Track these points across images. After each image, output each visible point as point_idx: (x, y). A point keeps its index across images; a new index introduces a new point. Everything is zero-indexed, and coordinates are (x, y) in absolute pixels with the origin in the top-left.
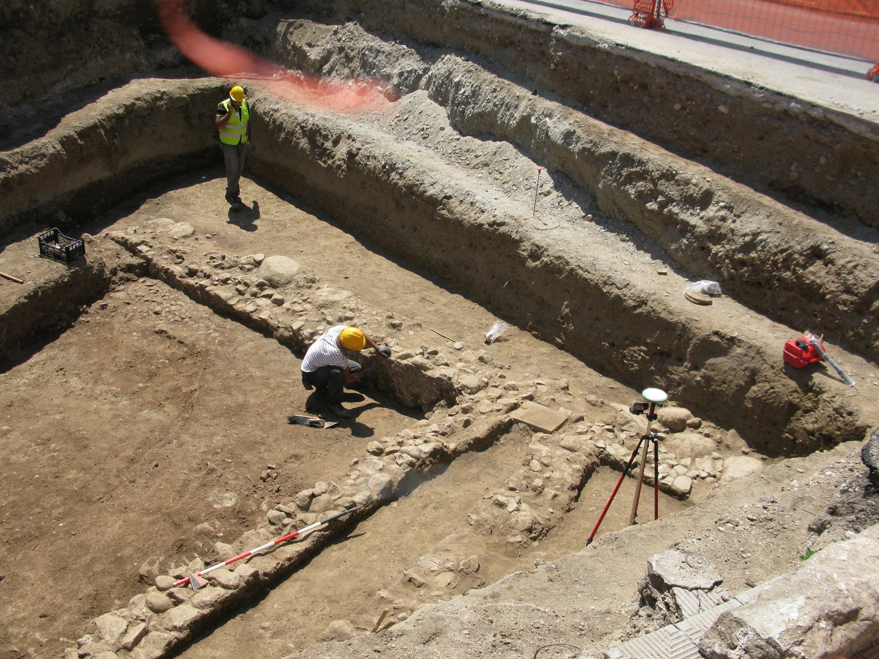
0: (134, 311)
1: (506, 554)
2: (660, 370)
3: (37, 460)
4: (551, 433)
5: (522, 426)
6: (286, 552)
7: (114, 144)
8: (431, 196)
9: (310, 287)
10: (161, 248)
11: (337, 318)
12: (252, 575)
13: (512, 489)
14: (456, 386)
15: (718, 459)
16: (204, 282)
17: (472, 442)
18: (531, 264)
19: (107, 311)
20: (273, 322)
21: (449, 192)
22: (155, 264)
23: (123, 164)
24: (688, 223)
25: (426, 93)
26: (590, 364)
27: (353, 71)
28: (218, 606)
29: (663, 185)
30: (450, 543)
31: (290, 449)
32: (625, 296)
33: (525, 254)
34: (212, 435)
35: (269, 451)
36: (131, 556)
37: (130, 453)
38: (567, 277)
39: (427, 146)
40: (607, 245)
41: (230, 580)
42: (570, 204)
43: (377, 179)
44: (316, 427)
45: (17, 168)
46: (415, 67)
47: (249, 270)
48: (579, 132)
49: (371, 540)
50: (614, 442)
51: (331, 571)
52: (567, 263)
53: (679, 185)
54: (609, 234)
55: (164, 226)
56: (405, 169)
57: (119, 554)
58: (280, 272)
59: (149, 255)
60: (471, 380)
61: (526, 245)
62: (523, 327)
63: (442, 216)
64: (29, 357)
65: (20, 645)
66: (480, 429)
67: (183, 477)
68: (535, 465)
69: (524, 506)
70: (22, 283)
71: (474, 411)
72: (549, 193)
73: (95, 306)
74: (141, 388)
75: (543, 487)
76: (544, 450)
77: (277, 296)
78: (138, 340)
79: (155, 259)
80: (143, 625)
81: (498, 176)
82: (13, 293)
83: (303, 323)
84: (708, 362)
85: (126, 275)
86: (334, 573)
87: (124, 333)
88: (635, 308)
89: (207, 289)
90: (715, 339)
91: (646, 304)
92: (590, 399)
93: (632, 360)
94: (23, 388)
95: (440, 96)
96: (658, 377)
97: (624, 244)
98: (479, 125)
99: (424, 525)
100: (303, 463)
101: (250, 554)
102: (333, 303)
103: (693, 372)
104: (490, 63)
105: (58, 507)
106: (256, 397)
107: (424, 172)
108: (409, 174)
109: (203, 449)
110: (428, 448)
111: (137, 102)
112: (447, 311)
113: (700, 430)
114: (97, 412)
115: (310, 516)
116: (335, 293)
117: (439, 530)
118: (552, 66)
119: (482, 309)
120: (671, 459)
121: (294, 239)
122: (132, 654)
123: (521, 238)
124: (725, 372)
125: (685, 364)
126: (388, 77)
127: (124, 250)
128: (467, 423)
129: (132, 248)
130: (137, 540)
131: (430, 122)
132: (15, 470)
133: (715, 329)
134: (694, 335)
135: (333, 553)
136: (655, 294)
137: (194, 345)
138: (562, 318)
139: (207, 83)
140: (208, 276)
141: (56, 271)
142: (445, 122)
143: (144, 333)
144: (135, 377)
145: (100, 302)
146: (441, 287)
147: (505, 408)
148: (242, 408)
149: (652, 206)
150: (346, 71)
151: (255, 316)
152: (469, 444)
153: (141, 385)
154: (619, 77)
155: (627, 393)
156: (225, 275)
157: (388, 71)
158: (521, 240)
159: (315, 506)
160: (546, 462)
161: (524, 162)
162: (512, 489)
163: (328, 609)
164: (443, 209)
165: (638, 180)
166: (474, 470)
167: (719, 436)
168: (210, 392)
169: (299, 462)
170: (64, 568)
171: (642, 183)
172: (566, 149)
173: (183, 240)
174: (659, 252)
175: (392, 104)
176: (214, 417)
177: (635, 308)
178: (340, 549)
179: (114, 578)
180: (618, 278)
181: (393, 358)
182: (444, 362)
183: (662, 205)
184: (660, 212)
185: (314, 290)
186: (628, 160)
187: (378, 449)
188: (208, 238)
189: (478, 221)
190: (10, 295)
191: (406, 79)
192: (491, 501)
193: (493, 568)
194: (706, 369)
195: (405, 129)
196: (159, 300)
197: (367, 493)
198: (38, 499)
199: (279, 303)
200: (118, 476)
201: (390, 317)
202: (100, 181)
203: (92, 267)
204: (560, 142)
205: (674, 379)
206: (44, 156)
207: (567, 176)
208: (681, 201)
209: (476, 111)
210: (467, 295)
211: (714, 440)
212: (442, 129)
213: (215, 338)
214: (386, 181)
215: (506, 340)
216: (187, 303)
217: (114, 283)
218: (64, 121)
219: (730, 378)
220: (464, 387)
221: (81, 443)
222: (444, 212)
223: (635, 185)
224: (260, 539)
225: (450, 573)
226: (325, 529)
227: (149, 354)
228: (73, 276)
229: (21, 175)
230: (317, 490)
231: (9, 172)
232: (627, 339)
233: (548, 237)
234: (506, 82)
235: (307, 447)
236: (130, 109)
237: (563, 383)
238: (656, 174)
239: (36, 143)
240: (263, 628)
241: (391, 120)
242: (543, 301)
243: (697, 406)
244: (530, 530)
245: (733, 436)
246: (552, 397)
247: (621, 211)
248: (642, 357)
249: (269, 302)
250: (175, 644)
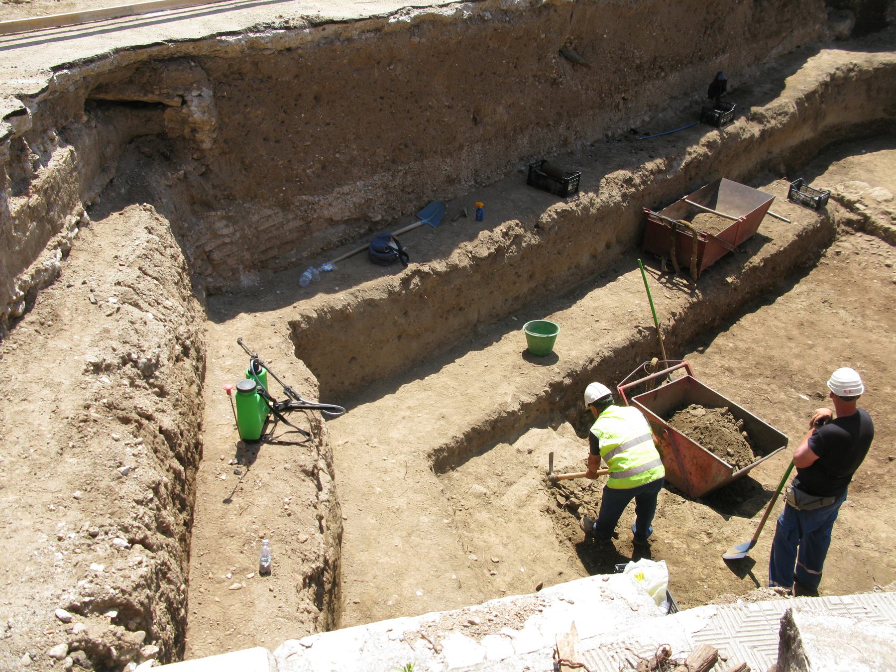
19: (840, 257)
22: (874, 222)
59: (868, 212)
79: (874, 218)
139: (888, 58)
206: (786, 113)
228: (822, 222)
229: (772, 128)
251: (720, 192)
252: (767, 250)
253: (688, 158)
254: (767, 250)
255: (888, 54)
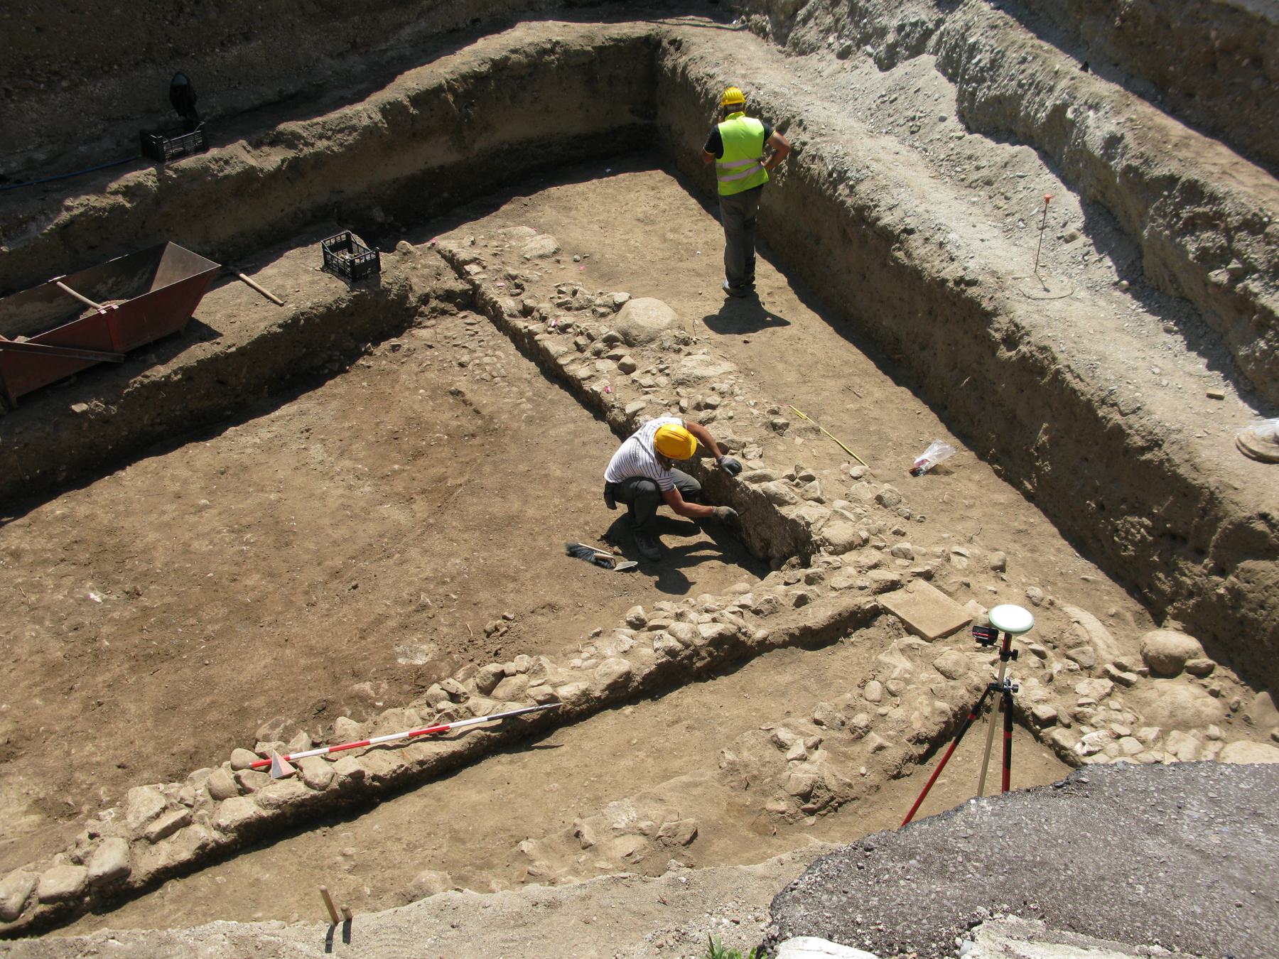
0: (433, 358)
1: (754, 827)
2: (1166, 564)
3: (220, 552)
4: (930, 640)
5: (891, 619)
6: (421, 751)
7: (468, 115)
8: (885, 227)
9: (679, 351)
10: (498, 271)
11: (694, 403)
12: (351, 775)
13: (818, 723)
14: (815, 538)
15: (1216, 739)
16: (534, 326)
17: (797, 633)
18: (1004, 353)
19: (397, 354)
20: (608, 398)
21: (911, 222)
22: (483, 294)
23: (481, 144)
24: (1271, 312)
25: (934, 58)
26: (1066, 534)
27: (838, 21)
28: (288, 810)
29: (1243, 241)
30: (672, 790)
31: (546, 594)
32: (1130, 428)
33: (998, 336)
34: (450, 555)
35: (518, 592)
36: (259, 709)
37: (338, 562)
38: (1050, 382)
39: (912, 146)
40: (1139, 336)
41: (317, 775)
42: (1100, 260)
43: (821, 193)
44: (603, 566)
45: (312, 145)
46: (924, 17)
47: (603, 315)
48: (1129, 139)
49: (564, 759)
50: (1033, 675)
51: (480, 792)
52: (1054, 359)
53: (1269, 244)
54: (1148, 318)
55: (521, 238)
56: (859, 181)
57: (246, 704)
58: (642, 323)
59: (477, 280)
60: (839, 532)
61: (1002, 322)
62: (982, 456)
63: (896, 260)
64: (276, 407)
65: (79, 798)
66: (817, 615)
67: (379, 610)
68: (874, 689)
69: (818, 755)
70: (282, 305)
71: (824, 583)
72: (1072, 238)
73: (385, 345)
74: (394, 472)
75: (868, 729)
76: (902, 664)
77: (627, 360)
78: (421, 401)
80: (184, 812)
81: (1002, 203)
82: (266, 318)
83: (643, 405)
84: (1241, 565)
85: (442, 305)
86: (485, 796)
87: (409, 389)
88: (1143, 450)
89: (537, 338)
90: (1260, 526)
91: (1160, 446)
92: (1031, 593)
93: (1126, 538)
94: (249, 451)
95: (951, 67)
96: (1161, 575)
97: (1168, 338)
98: (993, 117)
99: (658, 753)
100: (557, 618)
101: (368, 743)
102: (699, 380)
103: (1215, 578)
104: (1032, 14)
105: (217, 621)
106: (539, 508)
107: (884, 187)
108: (863, 188)
109: (429, 573)
110: (709, 631)
111: (513, 56)
112: (876, 412)
113: (1206, 681)
114: (323, 497)
115: (485, 704)
116: (709, 364)
117: (677, 764)
118: (1117, 22)
119: (933, 416)
120: (1122, 723)
121: (699, 275)
122: (153, 848)
123: (996, 309)
124: (1267, 588)
125: (1206, 561)
126: (882, 32)
127: (449, 269)
128: (801, 601)
129: (458, 266)
130: (278, 688)
131: (928, 107)
132: (191, 561)
133: (1264, 509)
134: (1226, 514)
135: (498, 766)
136: (1180, 431)
137: (492, 418)
138: (1037, 449)
139: (626, 31)
140: (544, 319)
141: (334, 290)
142: (948, 106)
143: (435, 392)
144: (394, 454)
145: (394, 341)
146: (886, 373)
147: (875, 586)
148: (512, 521)
149: (1219, 276)
150: (829, 20)
151: (587, 386)
152: (792, 635)
153: (396, 467)
154: (1217, 43)
155: (1109, 593)
156: (566, 318)
157: (884, 23)
158: (995, 313)
159: (499, 691)
160: (893, 688)
161: (1048, 181)
162: (818, 723)
163: (444, 850)
164: (899, 249)
165: (1205, 229)
166: (785, 678)
167: (1236, 698)
168: (476, 490)
169: (552, 616)
170: (174, 708)
171: (1209, 234)
172: (1107, 167)
173: (537, 262)
174: (1221, 358)
175: (882, 74)
176: (467, 529)
177: (1143, 450)
178: (511, 762)
179: (226, 735)
180: (1125, 396)
181: (739, 478)
182: (815, 496)
183: (1236, 277)
184: (1227, 290)
185: (682, 355)
186: (1194, 192)
187: (637, 619)
188: (576, 261)
189: (942, 274)
190: (260, 320)
191: (908, 35)
192: (768, 736)
193: (720, 844)
194: (1237, 577)
195: (889, 115)
196: (472, 345)
197: (583, 685)
198: (199, 607)
199: (628, 369)
200: (307, 593)
201: (774, 412)
202: (442, 168)
203: (390, 290)
204: (1098, 153)
205: (1183, 582)
206: (354, 128)
207: (1109, 212)
208: (1267, 272)
209: (993, 93)
210: (917, 393)
211: (1225, 705)
212: (943, 119)
213: (524, 411)
214: (831, 196)
215: (947, 473)
216: (507, 355)
217: (422, 314)
218: (399, 80)
219: (1273, 600)
220: (825, 541)
221: (283, 537)
222: (900, 254)
223: (1198, 237)
224: (401, 724)
225: (641, 840)
226: (493, 729)
227: (427, 423)
228: (356, 301)
229: (316, 154)
230: (509, 667)
231: (301, 150)
232: (1124, 501)
233: (1039, 311)
234: (1046, 46)
235: (574, 594)
236: (499, 66)
237: (995, 559)
238: (1234, 221)
239: (347, 110)
240: (344, 855)
241: (870, 101)
242: (1015, 417)
243: (1215, 637)
244: (806, 797)
245: (1263, 703)
246: (965, 580)
247: (1174, 279)
248: (1143, 536)
249: (612, 365)
250: (213, 849)
251: (162, 264)
252: (199, 352)
253: (64, 216)
254: (199, 352)
255: (536, 24)
